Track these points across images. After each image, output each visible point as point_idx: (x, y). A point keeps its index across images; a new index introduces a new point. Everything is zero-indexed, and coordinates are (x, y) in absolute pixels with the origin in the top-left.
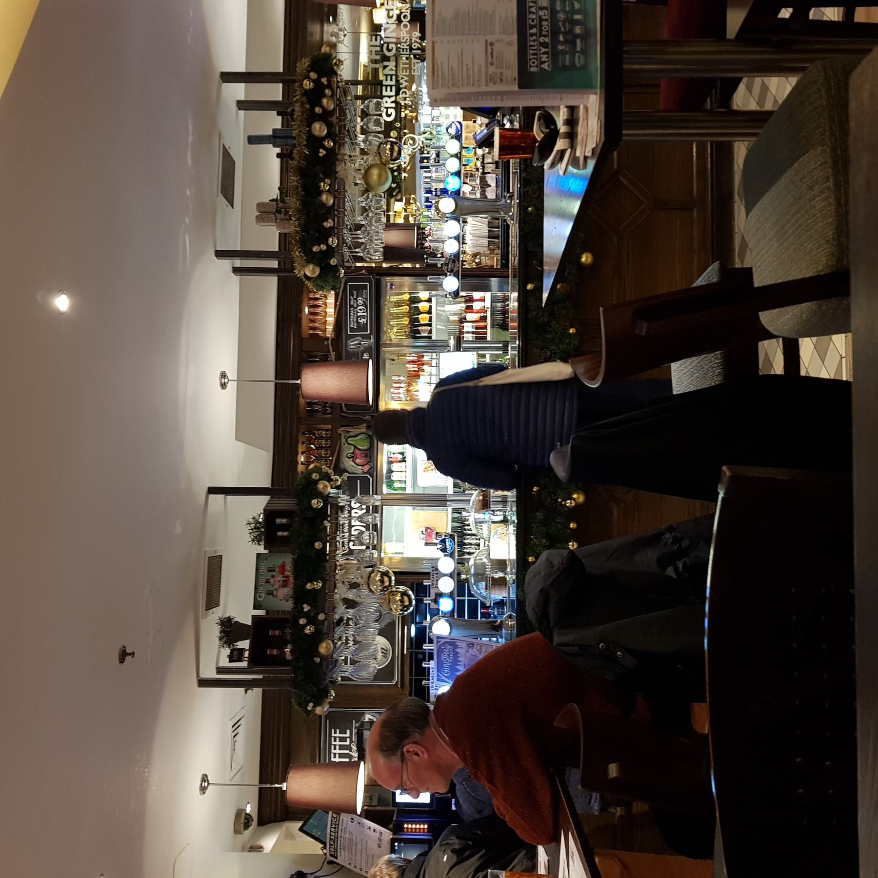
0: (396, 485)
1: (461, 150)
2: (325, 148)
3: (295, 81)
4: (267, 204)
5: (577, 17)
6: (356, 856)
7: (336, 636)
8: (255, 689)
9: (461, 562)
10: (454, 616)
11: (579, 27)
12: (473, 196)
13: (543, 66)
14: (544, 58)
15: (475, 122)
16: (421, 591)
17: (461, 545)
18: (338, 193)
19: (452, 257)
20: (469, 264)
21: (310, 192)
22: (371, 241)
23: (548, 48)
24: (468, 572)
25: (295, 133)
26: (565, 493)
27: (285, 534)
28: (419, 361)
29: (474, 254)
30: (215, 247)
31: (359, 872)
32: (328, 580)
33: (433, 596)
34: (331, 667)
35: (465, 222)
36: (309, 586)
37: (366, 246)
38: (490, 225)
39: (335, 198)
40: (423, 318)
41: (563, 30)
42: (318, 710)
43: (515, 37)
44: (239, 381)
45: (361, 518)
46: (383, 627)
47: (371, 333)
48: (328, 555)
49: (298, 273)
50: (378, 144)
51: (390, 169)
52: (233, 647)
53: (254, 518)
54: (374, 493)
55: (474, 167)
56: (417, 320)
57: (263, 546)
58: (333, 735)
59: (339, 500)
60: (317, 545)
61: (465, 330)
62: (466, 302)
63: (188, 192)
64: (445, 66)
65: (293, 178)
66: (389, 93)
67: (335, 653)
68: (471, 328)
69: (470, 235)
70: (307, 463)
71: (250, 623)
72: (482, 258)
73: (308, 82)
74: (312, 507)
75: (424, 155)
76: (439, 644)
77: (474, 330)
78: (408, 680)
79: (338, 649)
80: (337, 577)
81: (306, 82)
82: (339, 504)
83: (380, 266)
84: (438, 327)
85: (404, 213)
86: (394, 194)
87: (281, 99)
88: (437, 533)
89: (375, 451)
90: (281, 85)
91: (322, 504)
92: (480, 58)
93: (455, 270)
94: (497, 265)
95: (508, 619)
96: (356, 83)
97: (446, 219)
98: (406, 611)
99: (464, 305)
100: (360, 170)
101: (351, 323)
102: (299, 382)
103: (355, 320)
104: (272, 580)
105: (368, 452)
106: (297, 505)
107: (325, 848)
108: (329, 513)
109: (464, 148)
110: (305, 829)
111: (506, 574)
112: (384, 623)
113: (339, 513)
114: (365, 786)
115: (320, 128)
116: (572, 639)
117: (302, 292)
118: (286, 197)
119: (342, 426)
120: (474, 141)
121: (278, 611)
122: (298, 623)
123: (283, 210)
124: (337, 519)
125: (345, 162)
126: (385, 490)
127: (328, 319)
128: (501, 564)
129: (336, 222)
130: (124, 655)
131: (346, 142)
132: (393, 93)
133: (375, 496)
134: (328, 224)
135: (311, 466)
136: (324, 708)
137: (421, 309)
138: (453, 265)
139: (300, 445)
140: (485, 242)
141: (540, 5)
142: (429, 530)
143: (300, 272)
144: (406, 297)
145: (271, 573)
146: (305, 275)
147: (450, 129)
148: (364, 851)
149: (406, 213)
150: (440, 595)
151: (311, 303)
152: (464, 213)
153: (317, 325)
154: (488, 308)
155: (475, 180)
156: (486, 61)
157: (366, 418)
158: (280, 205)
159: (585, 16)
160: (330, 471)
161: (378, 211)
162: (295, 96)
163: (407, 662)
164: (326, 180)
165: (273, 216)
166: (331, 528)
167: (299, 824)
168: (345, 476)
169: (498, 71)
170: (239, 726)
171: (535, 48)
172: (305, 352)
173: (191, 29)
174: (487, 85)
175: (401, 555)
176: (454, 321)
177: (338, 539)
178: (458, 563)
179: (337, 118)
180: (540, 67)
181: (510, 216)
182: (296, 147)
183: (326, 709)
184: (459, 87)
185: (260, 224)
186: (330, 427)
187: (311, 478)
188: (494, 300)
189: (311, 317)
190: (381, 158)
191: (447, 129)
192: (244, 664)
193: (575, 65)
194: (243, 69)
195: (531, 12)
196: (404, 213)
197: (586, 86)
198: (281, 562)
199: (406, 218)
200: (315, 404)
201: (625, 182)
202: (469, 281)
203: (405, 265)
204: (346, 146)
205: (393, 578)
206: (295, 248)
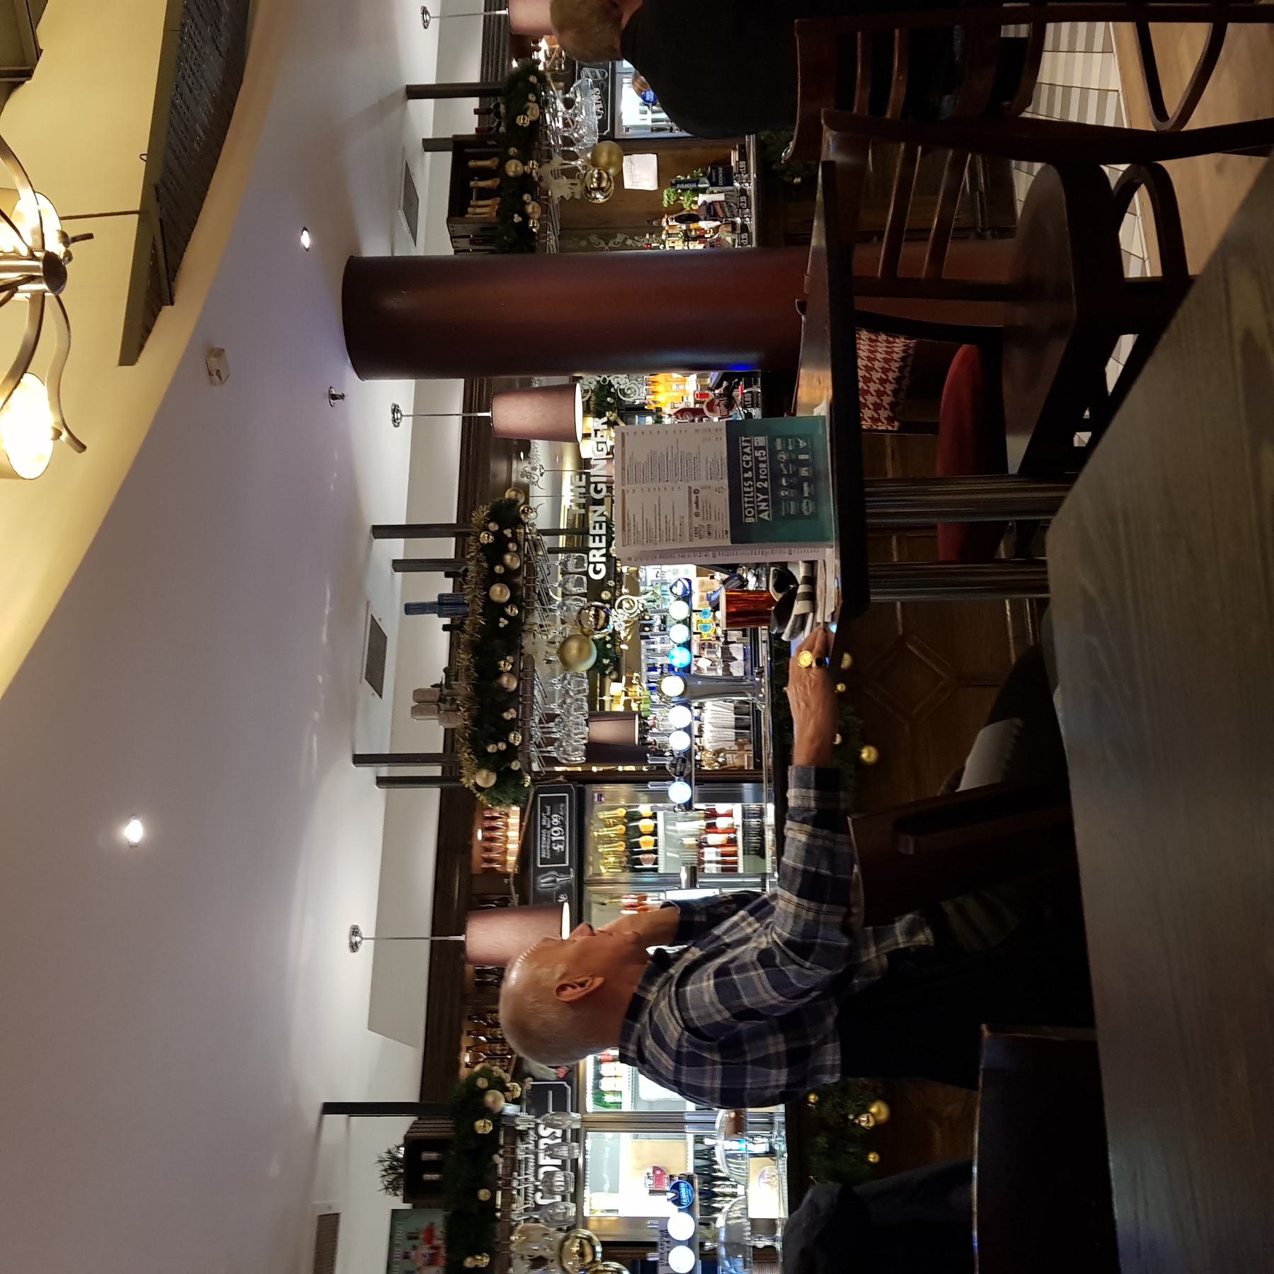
0: (608, 1099)
1: (691, 615)
2: (506, 617)
3: (469, 534)
4: (427, 691)
5: (802, 457)
9: (705, 1223)
12: (712, 674)
13: (761, 516)
14: (763, 506)
15: (712, 577)
17: (709, 1196)
18: (525, 674)
19: (682, 756)
20: (710, 765)
22: (569, 735)
23: (767, 494)
24: (715, 1238)
26: (858, 1106)
27: (435, 1177)
28: (641, 905)
29: (716, 751)
30: (353, 750)
35: (700, 707)
36: (469, 1262)
37: (561, 742)
38: (737, 711)
39: (519, 679)
40: (646, 842)
43: (726, 482)
45: (551, 1150)
47: (570, 866)
49: (467, 782)
50: (579, 608)
51: (593, 640)
53: (389, 1152)
54: (575, 1109)
55: (713, 635)
56: (637, 845)
60: (484, 1194)
61: (706, 858)
62: (707, 817)
63: (320, 679)
64: (639, 519)
65: (462, 656)
66: (597, 544)
68: (714, 855)
69: (710, 725)
70: (475, 1062)
75: (645, 622)
77: (720, 858)
80: (513, 1248)
82: (518, 1128)
83: (588, 769)
84: (669, 854)
85: (623, 698)
86: (607, 672)
90: (453, 539)
92: (683, 509)
93: (686, 772)
94: (748, 766)
96: (555, 532)
97: (672, 705)
99: (703, 823)
100: (554, 643)
101: (543, 852)
102: (462, 938)
103: (548, 847)
109: (695, 611)
111: (775, 1241)
115: (501, 591)
117: (474, 809)
118: (456, 680)
120: (708, 603)
123: (449, 698)
124: (514, 1151)
126: (590, 1106)
127: (509, 846)
128: (771, 1224)
129: (520, 712)
132: (603, 544)
133: (574, 1115)
134: (509, 715)
135: (478, 1068)
137: (642, 830)
138: (686, 766)
140: (731, 734)
141: (756, 444)
143: (468, 780)
144: (622, 812)
146: (476, 784)
147: (674, 588)
149: (626, 698)
151: (487, 824)
152: (698, 694)
153: (494, 855)
154: (738, 826)
155: (715, 652)
158: (446, 691)
159: (813, 455)
160: (507, 1077)
161: (579, 696)
164: (508, 658)
165: (435, 707)
168: (529, 1082)
169: (705, 524)
171: (752, 494)
176: (690, 846)
177: (515, 1184)
178: (700, 1224)
179: (525, 578)
180: (759, 518)
181: (760, 699)
182: (468, 616)
184: (656, 544)
185: (417, 717)
187: (475, 1086)
188: (745, 814)
189: (487, 844)
191: (671, 588)
193: (802, 513)
194: (402, 521)
195: (745, 453)
196: (623, 698)
197: (818, 538)
200: (489, 972)
201: (916, 652)
202: (708, 788)
203: (628, 768)
204: (536, 613)
205: (599, 1249)
206: (463, 749)
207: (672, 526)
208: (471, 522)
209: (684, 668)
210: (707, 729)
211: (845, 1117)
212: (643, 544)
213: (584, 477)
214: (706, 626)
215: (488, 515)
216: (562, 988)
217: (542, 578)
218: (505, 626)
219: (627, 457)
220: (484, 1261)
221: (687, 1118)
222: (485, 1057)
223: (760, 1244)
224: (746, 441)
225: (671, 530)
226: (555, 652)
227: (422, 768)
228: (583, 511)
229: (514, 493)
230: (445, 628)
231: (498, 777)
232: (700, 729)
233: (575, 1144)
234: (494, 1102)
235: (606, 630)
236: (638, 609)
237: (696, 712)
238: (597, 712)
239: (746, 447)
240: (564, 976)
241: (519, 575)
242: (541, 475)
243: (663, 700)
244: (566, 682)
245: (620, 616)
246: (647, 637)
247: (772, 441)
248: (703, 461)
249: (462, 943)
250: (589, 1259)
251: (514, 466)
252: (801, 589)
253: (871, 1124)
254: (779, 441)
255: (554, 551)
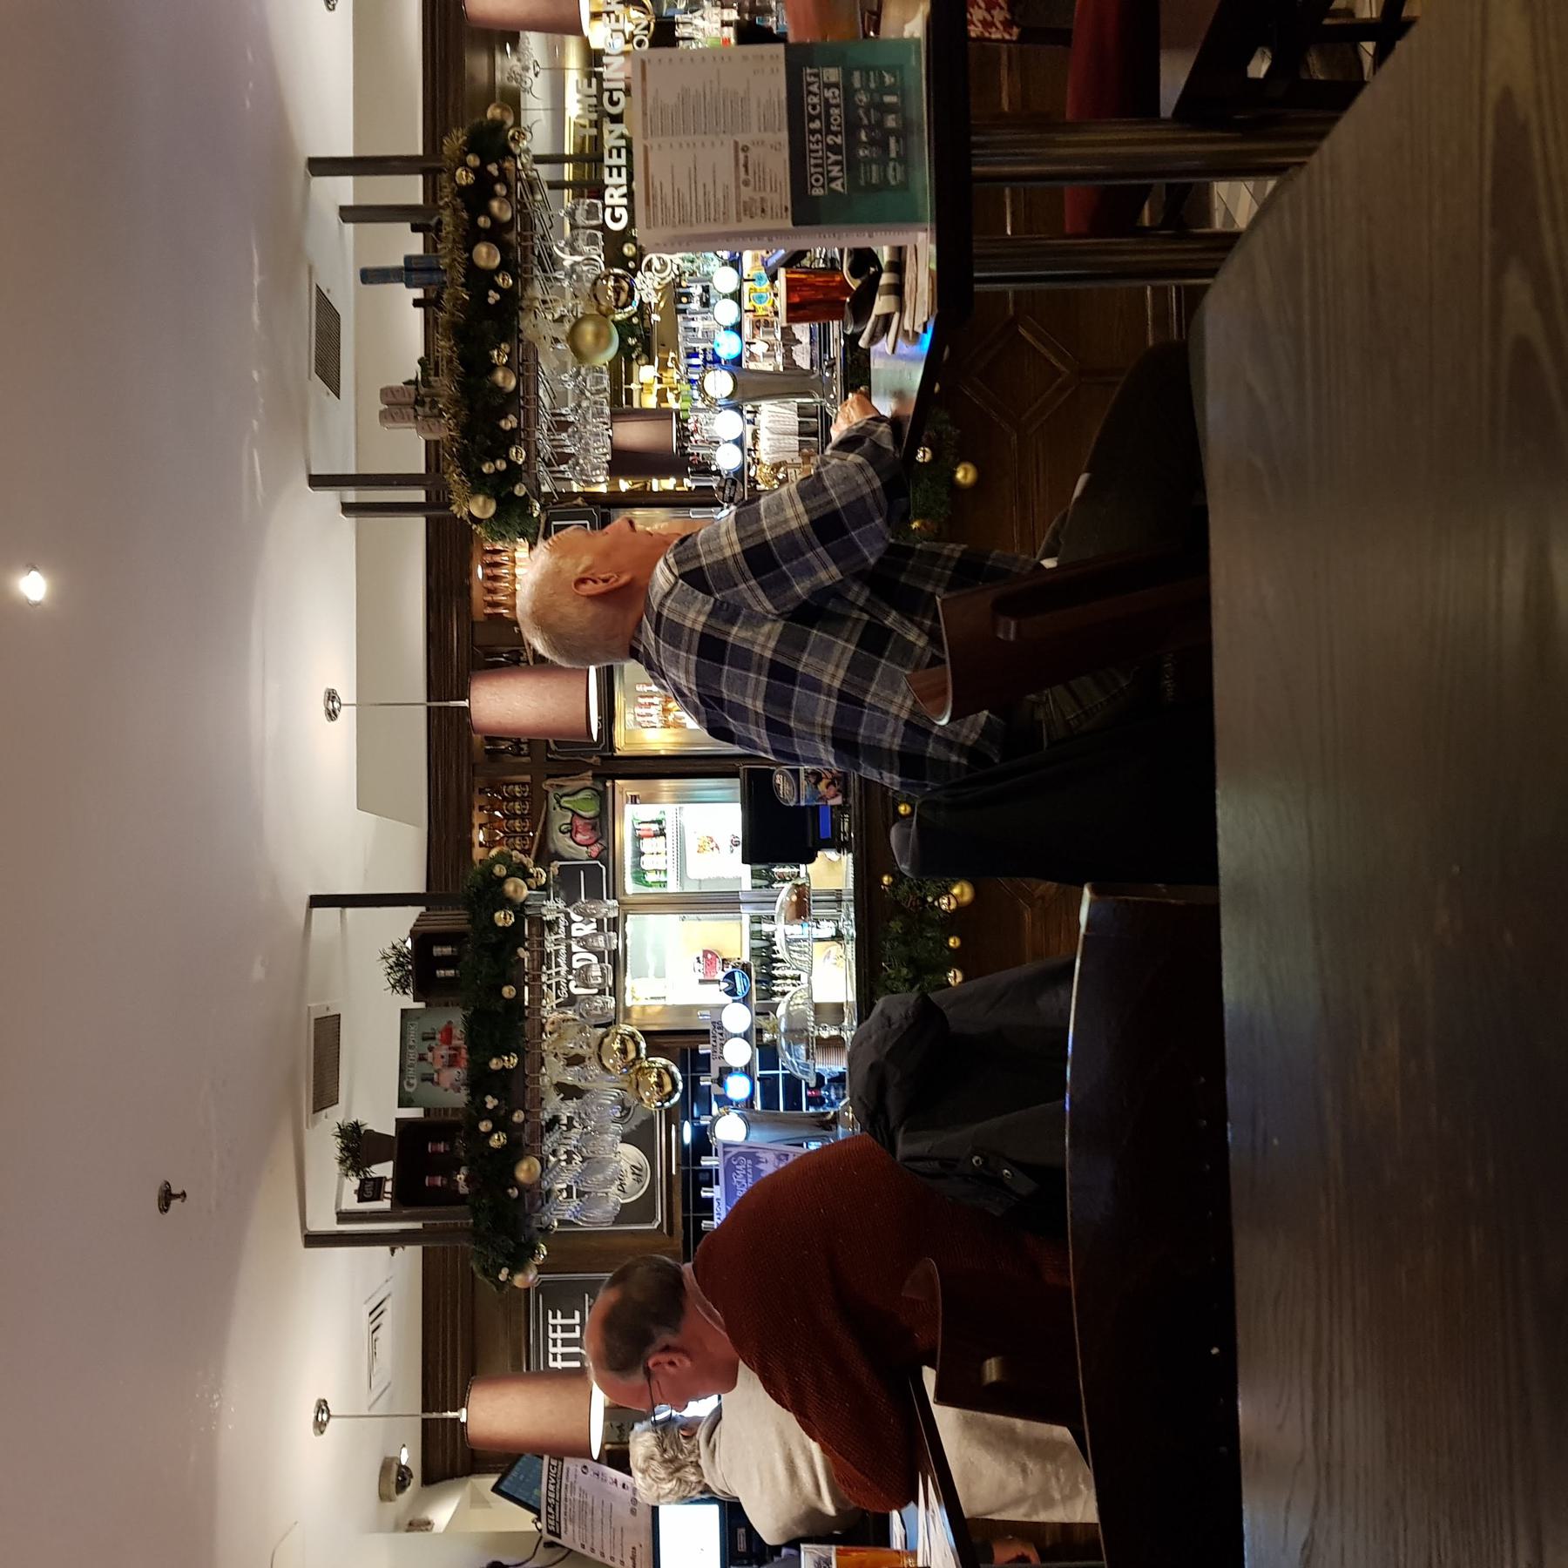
0: (650, 877)
2: (498, 289)
3: (440, 171)
4: (399, 389)
5: (888, 99)
6: (593, 1531)
7: (547, 1149)
8: (407, 1248)
10: (752, 1106)
11: (893, 116)
13: (833, 185)
16: (695, 1064)
18: (525, 366)
19: (732, 476)
20: (767, 482)
21: (474, 368)
23: (841, 154)
24: (775, 1029)
25: (444, 263)
27: (451, 973)
29: (774, 464)
30: (308, 468)
31: (600, 1559)
32: (527, 1052)
33: (715, 1073)
34: (539, 1203)
36: (495, 1064)
39: (519, 376)
41: (865, 121)
42: (519, 1281)
43: (784, 136)
44: (359, 705)
46: (633, 1128)
48: (527, 1007)
50: (594, 277)
51: (613, 321)
52: (365, 1174)
54: (611, 896)
55: (771, 309)
57: (412, 996)
58: (551, 1321)
59: (544, 911)
60: (508, 991)
63: (256, 375)
64: (668, 190)
65: (442, 343)
67: (544, 1179)
70: (490, 844)
71: (392, 1133)
72: (789, 471)
73: (464, 173)
74: (496, 925)
76: (729, 1156)
78: (680, 1220)
79: (550, 1171)
80: (544, 1046)
81: (460, 172)
85: (657, 386)
86: (634, 356)
87: (420, 201)
88: (724, 960)
89: (610, 819)
91: (513, 920)
92: (726, 176)
95: (842, 1106)
96: (558, 159)
97: (719, 409)
98: (668, 1100)
102: (465, 703)
104: (430, 1054)
105: (597, 820)
106: (469, 921)
107: (539, 1519)
108: (526, 932)
109: (746, 280)
110: (503, 1488)
112: (633, 1124)
113: (546, 933)
114: (605, 1408)
115: (489, 254)
116: (927, 1150)
118: (437, 375)
119: (549, 777)
121: (446, 1110)
122: (479, 1129)
124: (541, 944)
125: (535, 313)
126: (631, 887)
128: (839, 1008)
130: (167, 1197)
131: (536, 276)
132: (623, 180)
134: (508, 423)
135: (494, 852)
136: (526, 1275)
139: (476, 812)
140: (794, 442)
142: (709, 956)
143: (460, 508)
145: (427, 1044)
146: (470, 513)
148: (607, 1521)
150: (727, 1071)
151: (488, 559)
153: (501, 598)
156: (737, 178)
157: (592, 761)
158: (423, 390)
160: (529, 861)
161: (597, 398)
162: (442, 198)
163: (678, 1187)
166: (531, 960)
167: (492, 1480)
169: (757, 196)
170: (382, 1312)
171: (820, 153)
172: (478, 647)
173: (251, 85)
174: (739, 220)
175: (662, 1002)
177: (544, 978)
178: (757, 1014)
179: (518, 234)
180: (830, 189)
183: (531, 1277)
184: (691, 225)
186: (527, 778)
187: (492, 873)
189: (489, 584)
190: (599, 304)
192: (385, 1204)
193: (888, 182)
194: (348, 152)
195: (810, 93)
196: (657, 386)
197: (908, 219)
198: (445, 1023)
199: (662, 395)
204: (536, 283)
205: (643, 1045)
206: (451, 468)
207: (712, 199)
208: (442, 153)
209: (733, 360)
210: (764, 435)
211: (924, 901)
212: (674, 226)
213: (594, 81)
214: (762, 297)
215: (465, 144)
216: (582, 581)
217: (542, 233)
218: (496, 302)
219: (650, 101)
220: (512, 1061)
221: (742, 898)
222: (502, 835)
223: (825, 1035)
224: (811, 75)
225: (712, 204)
226: (564, 338)
227: (398, 492)
228: (594, 132)
229: (498, 111)
230: (417, 303)
231: (498, 505)
232: (755, 437)
233: (612, 934)
234: (516, 891)
235: (630, 308)
236: (669, 275)
237: (749, 416)
238: (622, 407)
239: (813, 83)
240: (585, 571)
241: (512, 230)
242: (536, 75)
243: (707, 402)
244: (580, 378)
245: (648, 282)
246: (684, 311)
247: (847, 75)
248: (754, 105)
249: (466, 711)
250: (632, 1055)
251: (498, 58)
252: (885, 279)
253: (953, 907)
254: (857, 75)
255: (557, 185)
